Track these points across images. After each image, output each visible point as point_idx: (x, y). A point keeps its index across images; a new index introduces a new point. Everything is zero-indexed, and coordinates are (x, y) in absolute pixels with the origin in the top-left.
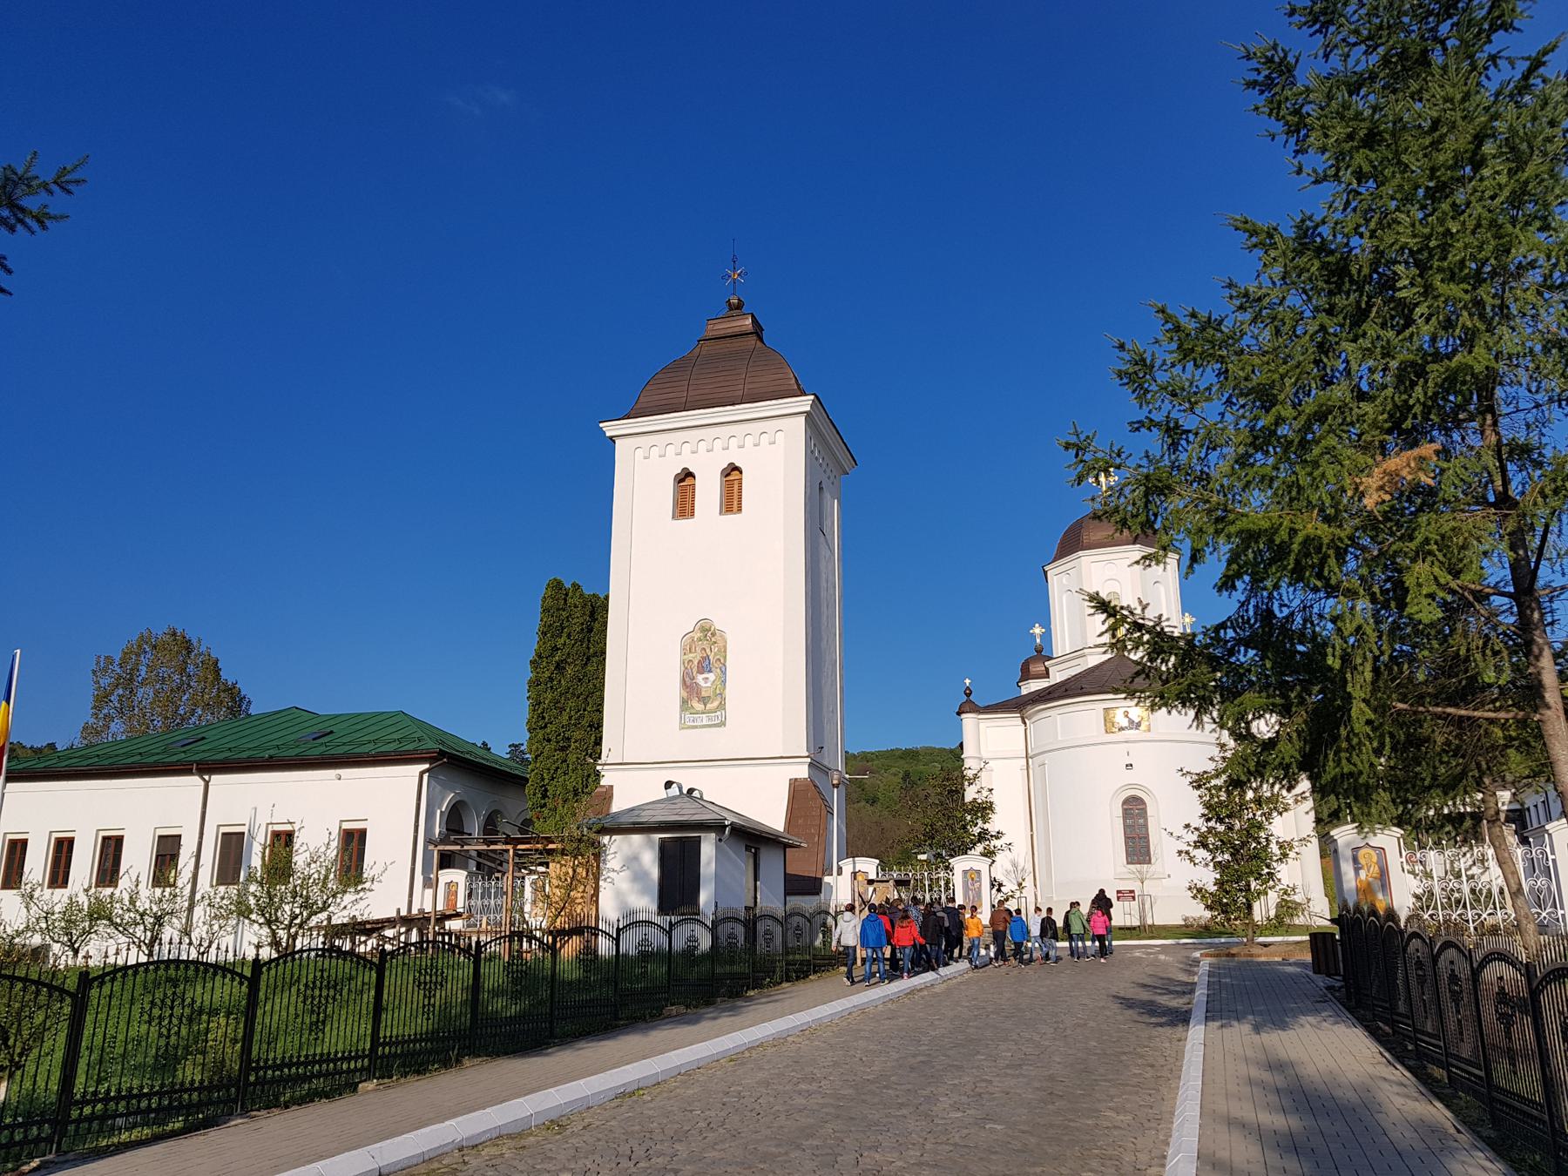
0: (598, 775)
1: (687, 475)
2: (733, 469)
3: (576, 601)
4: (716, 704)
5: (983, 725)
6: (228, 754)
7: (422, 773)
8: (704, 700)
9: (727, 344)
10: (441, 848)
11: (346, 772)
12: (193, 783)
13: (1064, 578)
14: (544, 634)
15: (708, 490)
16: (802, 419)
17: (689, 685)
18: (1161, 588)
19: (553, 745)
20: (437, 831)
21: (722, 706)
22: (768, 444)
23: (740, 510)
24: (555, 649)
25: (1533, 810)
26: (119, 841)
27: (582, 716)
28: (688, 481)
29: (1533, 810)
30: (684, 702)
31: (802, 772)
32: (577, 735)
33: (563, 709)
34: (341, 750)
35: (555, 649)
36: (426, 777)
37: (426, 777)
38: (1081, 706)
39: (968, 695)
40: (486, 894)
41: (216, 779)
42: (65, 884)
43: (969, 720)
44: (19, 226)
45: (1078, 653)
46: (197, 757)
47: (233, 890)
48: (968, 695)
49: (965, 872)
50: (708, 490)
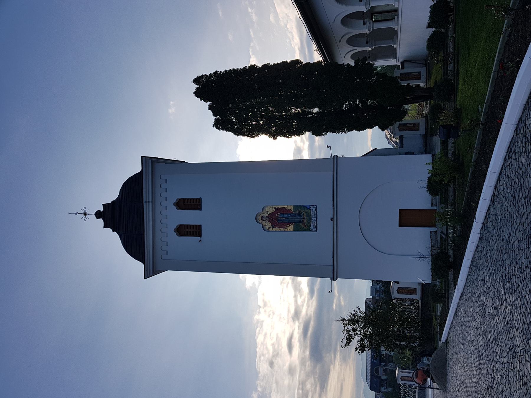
15: (189, 217)
50: (189, 217)
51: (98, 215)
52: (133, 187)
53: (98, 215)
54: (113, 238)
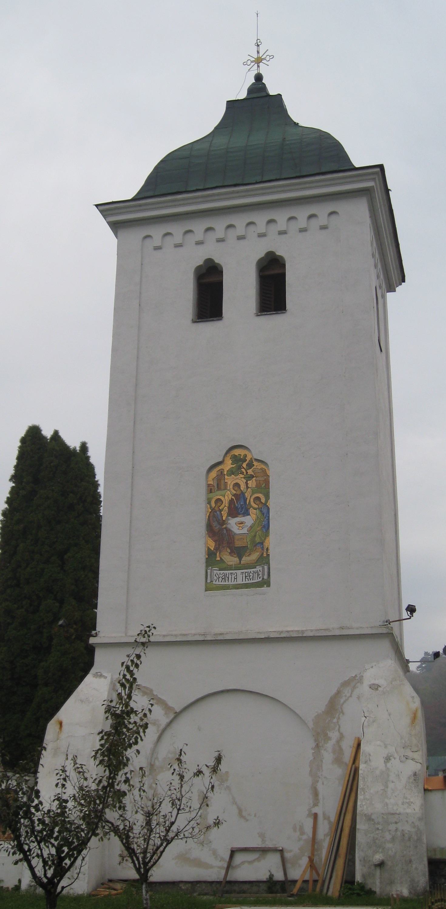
4: (255, 556)
8: (239, 552)
15: (240, 290)
17: (216, 529)
21: (264, 560)
50: (240, 290)
51: (258, 86)
52: (322, 156)
53: (258, 86)
54: (196, 120)
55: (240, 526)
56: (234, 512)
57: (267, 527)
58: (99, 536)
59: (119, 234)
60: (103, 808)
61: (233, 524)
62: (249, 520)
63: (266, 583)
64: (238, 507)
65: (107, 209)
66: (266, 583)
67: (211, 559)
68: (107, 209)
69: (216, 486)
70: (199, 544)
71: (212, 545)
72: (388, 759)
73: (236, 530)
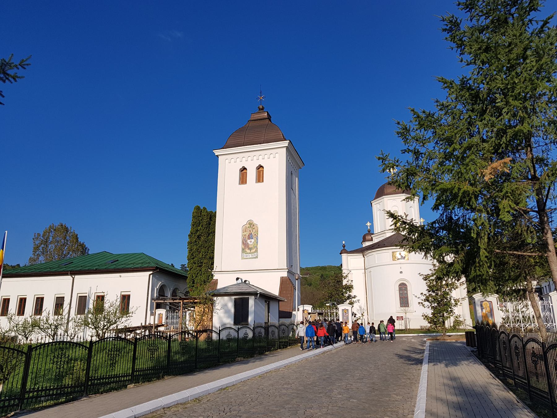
0: (212, 275)
1: (244, 169)
2: (261, 167)
3: (205, 213)
4: (254, 250)
5: (349, 258)
6: (81, 268)
7: (150, 275)
8: (250, 249)
9: (258, 122)
10: (157, 301)
11: (123, 275)
12: (69, 278)
13: (378, 205)
14: (193, 225)
15: (251, 174)
16: (285, 149)
17: (245, 243)
18: (413, 209)
19: (197, 265)
20: (155, 295)
21: (256, 251)
22: (273, 158)
23: (263, 181)
24: (197, 231)
25: (544, 288)
26: (42, 299)
27: (207, 255)
28: (244, 171)
29: (544, 288)
30: (243, 249)
31: (285, 274)
32: (205, 261)
33: (200, 252)
34: (121, 267)
35: (197, 231)
36: (151, 276)
37: (151, 276)
38: (384, 251)
39: (344, 247)
40: (173, 318)
41: (77, 277)
42: (23, 314)
43: (344, 256)
44: (7, 80)
45: (383, 232)
46: (70, 269)
47: (83, 316)
48: (344, 247)
49: (343, 310)
50: (251, 174)
55: (250, 242)
56: (249, 238)
57: (257, 242)
58: (213, 244)
59: (339, 265)
60: (442, 262)
61: (249, 241)
62: (253, 240)
63: (257, 257)
64: (250, 237)
65: (391, 317)
66: (257, 257)
67: (243, 250)
68: (391, 317)
69: (244, 230)
70: (240, 246)
71: (243, 247)
72: (92, 336)
73: (249, 243)
